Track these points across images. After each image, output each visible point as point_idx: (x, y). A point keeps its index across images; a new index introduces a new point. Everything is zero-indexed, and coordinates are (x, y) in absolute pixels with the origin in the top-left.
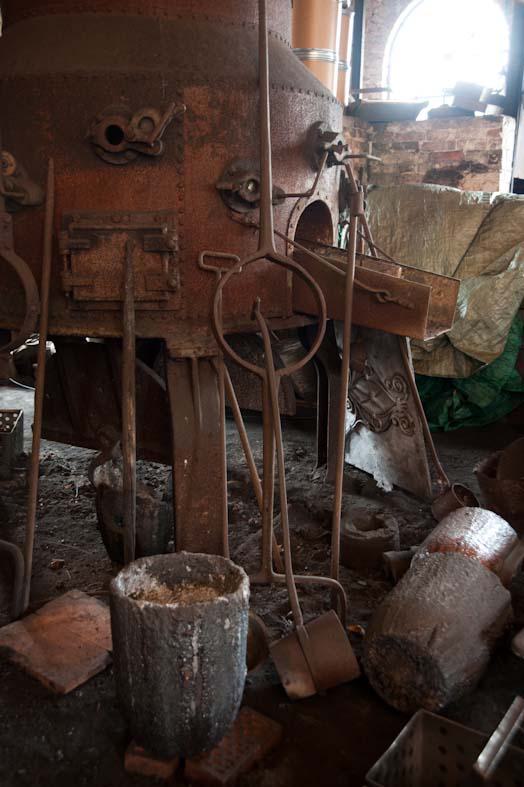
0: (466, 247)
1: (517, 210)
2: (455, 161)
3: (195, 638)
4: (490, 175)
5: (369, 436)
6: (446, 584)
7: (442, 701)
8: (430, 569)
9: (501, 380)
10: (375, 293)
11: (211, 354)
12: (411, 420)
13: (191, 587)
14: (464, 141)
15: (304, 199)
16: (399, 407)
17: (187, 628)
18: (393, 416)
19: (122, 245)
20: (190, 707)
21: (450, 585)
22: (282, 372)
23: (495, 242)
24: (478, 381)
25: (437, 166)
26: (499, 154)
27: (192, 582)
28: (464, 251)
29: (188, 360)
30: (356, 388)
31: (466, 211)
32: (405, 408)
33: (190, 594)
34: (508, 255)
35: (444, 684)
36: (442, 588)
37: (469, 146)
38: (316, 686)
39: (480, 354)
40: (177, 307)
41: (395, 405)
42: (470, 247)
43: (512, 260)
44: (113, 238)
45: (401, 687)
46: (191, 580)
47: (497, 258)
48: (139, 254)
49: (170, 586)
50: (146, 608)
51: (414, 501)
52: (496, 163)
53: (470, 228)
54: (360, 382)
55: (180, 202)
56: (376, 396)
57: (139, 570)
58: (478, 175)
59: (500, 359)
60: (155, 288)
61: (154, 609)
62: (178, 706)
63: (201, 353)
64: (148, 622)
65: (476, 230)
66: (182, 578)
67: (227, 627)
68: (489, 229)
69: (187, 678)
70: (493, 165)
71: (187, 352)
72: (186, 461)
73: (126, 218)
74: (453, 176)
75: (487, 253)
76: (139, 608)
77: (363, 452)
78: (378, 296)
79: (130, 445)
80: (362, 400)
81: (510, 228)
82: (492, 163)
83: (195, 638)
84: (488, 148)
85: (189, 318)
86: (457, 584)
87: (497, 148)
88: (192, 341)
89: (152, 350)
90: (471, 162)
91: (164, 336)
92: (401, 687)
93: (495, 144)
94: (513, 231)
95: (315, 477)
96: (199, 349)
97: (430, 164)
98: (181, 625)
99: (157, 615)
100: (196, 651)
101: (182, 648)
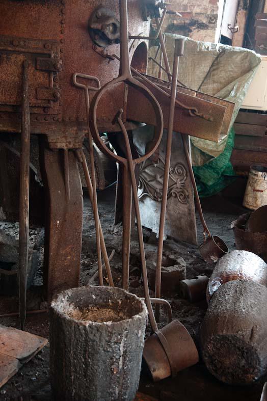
0: (202, 79)
1: (234, 57)
2: (187, 20)
3: (122, 344)
4: (209, 32)
5: (152, 204)
6: (251, 301)
7: (256, 376)
8: (236, 291)
9: (222, 168)
10: (188, 110)
11: (77, 147)
12: (187, 194)
13: (96, 309)
14: (194, 6)
15: (137, 40)
16: (179, 185)
17: (117, 338)
18: (173, 191)
19: (20, 63)
20: (115, 393)
21: (252, 301)
22: (138, 161)
23: (221, 77)
24: (207, 168)
25: (175, 22)
26: (216, 17)
27: (96, 305)
28: (201, 82)
29: (61, 151)
30: (145, 172)
31: (202, 55)
32: (183, 186)
33: (94, 314)
34: (230, 87)
35: (259, 364)
36: (249, 303)
37: (197, 10)
38: (171, 372)
39: (211, 151)
40: (56, 112)
41: (176, 184)
42: (204, 80)
43: (232, 90)
44: (13, 57)
45: (228, 368)
46: (96, 304)
47: (222, 88)
48: (32, 71)
49: (81, 309)
50: (90, 326)
51: (183, 247)
52: (213, 23)
53: (205, 67)
54: (148, 168)
55: (61, 35)
56: (160, 178)
57: (63, 300)
58: (202, 31)
59: (222, 154)
60: (44, 97)
61: (96, 326)
62: (108, 392)
63: (71, 146)
64: (91, 336)
65: (208, 68)
66: (89, 303)
67: (139, 335)
68: (217, 69)
69: (115, 373)
70: (212, 25)
71: (62, 145)
72: (58, 222)
73: (22, 43)
74: (185, 29)
75: (215, 85)
76: (85, 326)
77: (148, 214)
78: (190, 111)
79: (26, 211)
80: (148, 180)
81: (230, 69)
82: (211, 23)
83: (122, 344)
84: (209, 12)
85: (63, 120)
86: (256, 300)
87: (215, 13)
88: (65, 137)
89: (41, 141)
90: (198, 21)
91: (47, 133)
92: (228, 368)
93: (213, 10)
94: (232, 71)
95: (115, 231)
96: (70, 143)
97: (171, 20)
98: (114, 336)
99: (98, 330)
100: (122, 353)
101: (113, 352)
